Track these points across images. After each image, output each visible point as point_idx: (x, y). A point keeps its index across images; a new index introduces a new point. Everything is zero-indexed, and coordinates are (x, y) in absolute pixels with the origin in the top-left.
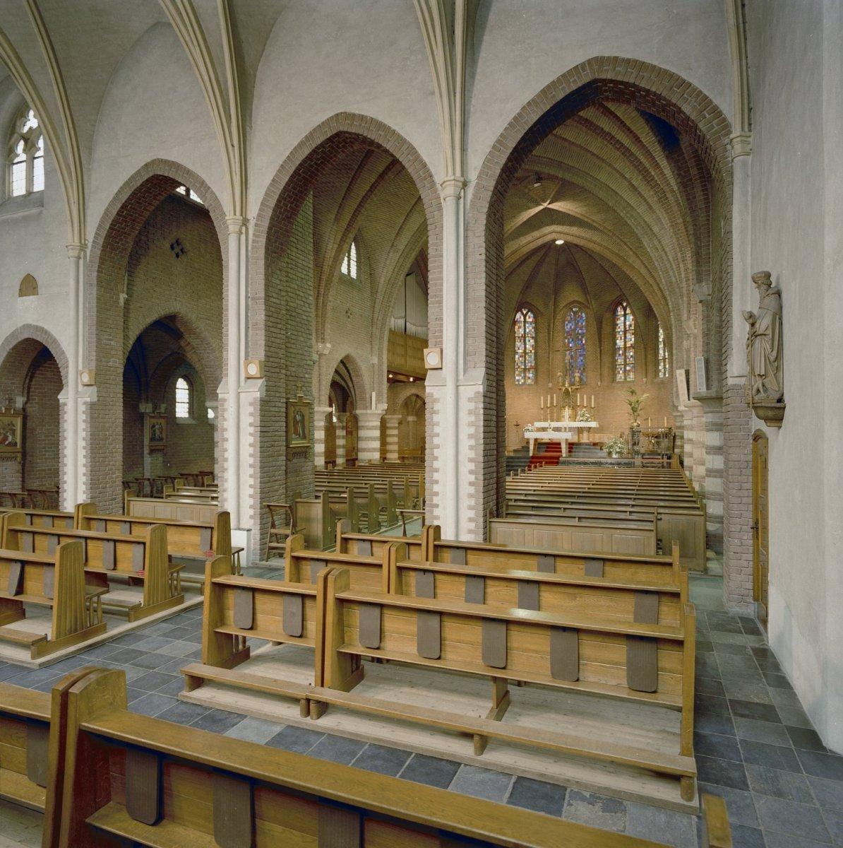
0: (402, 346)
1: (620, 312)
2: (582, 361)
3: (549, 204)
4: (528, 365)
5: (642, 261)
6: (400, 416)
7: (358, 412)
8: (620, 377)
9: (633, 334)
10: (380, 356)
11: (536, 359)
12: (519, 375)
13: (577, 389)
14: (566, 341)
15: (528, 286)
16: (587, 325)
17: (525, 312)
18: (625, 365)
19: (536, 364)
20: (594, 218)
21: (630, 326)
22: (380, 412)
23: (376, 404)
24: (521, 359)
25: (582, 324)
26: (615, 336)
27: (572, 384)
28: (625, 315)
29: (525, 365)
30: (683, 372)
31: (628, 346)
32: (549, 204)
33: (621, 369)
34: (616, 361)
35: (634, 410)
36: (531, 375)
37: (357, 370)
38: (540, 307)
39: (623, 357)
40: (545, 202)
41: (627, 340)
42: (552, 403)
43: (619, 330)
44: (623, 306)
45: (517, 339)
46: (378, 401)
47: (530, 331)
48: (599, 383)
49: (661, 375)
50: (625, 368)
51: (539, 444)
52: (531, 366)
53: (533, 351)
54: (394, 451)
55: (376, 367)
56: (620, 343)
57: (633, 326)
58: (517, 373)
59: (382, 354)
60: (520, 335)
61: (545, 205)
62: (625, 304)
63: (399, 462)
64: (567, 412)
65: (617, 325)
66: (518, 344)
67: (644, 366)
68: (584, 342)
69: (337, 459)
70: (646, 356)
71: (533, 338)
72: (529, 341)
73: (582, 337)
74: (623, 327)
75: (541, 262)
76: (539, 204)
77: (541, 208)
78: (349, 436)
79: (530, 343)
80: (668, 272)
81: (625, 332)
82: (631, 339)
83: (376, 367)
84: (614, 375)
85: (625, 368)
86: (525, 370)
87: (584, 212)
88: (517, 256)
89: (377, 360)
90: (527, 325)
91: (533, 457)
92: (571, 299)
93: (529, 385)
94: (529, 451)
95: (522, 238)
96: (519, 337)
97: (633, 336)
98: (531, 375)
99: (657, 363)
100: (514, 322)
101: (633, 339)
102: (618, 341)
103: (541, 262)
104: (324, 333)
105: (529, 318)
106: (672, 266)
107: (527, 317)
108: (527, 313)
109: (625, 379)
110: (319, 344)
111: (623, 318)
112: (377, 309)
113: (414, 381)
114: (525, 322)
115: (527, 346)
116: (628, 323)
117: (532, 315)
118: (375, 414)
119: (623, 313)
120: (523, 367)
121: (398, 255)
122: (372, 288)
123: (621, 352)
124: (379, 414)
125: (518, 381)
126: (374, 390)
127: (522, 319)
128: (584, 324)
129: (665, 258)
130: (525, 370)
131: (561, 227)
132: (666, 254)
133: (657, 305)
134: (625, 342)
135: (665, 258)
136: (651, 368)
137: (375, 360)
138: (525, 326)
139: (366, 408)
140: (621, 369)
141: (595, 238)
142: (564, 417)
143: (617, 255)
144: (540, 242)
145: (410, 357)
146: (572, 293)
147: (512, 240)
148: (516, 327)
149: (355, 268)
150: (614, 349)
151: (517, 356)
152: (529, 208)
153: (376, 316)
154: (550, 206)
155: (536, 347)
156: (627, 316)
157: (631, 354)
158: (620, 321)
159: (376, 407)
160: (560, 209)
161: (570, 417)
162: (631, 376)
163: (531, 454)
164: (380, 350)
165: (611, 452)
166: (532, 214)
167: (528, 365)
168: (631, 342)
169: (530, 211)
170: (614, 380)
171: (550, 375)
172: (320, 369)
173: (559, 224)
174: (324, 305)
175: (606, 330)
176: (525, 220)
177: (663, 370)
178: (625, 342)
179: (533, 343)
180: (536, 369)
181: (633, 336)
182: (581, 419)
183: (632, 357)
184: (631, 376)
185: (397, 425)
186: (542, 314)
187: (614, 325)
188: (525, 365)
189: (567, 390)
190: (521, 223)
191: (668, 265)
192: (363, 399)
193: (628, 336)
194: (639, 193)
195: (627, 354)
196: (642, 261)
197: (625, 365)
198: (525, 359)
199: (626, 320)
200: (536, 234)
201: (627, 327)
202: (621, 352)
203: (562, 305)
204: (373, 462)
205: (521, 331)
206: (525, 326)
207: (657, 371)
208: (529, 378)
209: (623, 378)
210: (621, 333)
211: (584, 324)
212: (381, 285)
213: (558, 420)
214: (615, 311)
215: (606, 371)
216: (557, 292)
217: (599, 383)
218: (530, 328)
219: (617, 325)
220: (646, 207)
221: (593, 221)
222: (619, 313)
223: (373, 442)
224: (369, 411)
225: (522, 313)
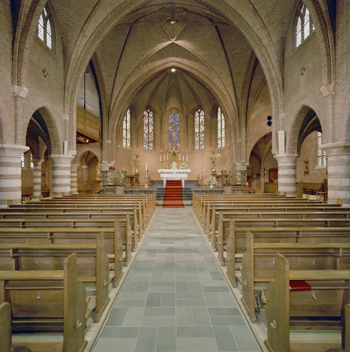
0: (83, 117)
1: (197, 114)
2: (177, 139)
3: (175, 40)
4: (150, 140)
5: (222, 81)
6: (79, 165)
7: (52, 156)
8: (197, 147)
9: (204, 126)
10: (71, 115)
11: (154, 136)
12: (146, 145)
13: (178, 152)
14: (170, 128)
15: (153, 95)
16: (180, 121)
17: (148, 111)
18: (200, 141)
19: (154, 139)
20: (199, 53)
21: (202, 121)
22: (71, 157)
23: (68, 151)
24: (146, 136)
25: (177, 120)
26: (194, 126)
27: (176, 149)
28: (199, 116)
29: (149, 140)
30: (283, 132)
31: (201, 132)
32: (175, 40)
33: (197, 143)
34: (195, 139)
35: (213, 162)
36: (152, 145)
37: (51, 122)
38: (157, 109)
39: (199, 137)
40: (173, 39)
41: (200, 129)
42: (163, 160)
43: (196, 124)
44: (198, 112)
45: (145, 126)
46: (69, 148)
47: (151, 121)
48: (186, 150)
49: (219, 146)
50: (200, 142)
51: (169, 182)
52: (152, 140)
53: (153, 132)
54: (284, 176)
55: (68, 123)
56: (197, 130)
57: (204, 122)
58: (144, 143)
59: (72, 113)
60: (146, 123)
61: (173, 40)
62: (199, 111)
63: (77, 193)
64: (174, 164)
65: (195, 121)
66: (145, 128)
67: (210, 142)
68: (178, 129)
69: (34, 193)
70: (211, 137)
71: (152, 125)
72: (151, 127)
73: (178, 127)
74: (198, 122)
75: (161, 82)
76: (169, 39)
77: (170, 42)
78: (44, 177)
79: (151, 128)
80: (271, 71)
81: (199, 125)
82: (203, 128)
83: (68, 123)
84: (194, 146)
85: (200, 142)
86: (149, 142)
87: (193, 49)
88: (152, 73)
89: (68, 117)
90: (150, 118)
91: (166, 189)
92: (173, 106)
93: (151, 150)
94: (163, 185)
95: (156, 62)
96: (145, 124)
97: (204, 127)
98: (152, 145)
99: (217, 140)
100: (144, 116)
101: (204, 128)
102: (196, 129)
103: (161, 82)
104: (20, 77)
105: (151, 114)
106: (273, 67)
107: (150, 114)
108: (149, 112)
109: (200, 148)
110: (15, 86)
111: (198, 118)
112: (68, 78)
113: (89, 142)
114: (148, 116)
115: (150, 129)
116: (201, 120)
117: (152, 113)
118: (68, 158)
119: (198, 115)
120: (148, 140)
121: (86, 40)
122: (64, 62)
123: (197, 135)
124: (70, 158)
125: (145, 148)
126: (65, 140)
127: (147, 115)
128: (178, 120)
129: (269, 61)
130: (149, 142)
131: (178, 58)
132: (270, 59)
133: (228, 106)
134: (199, 130)
135: (269, 61)
136: (213, 143)
137: (67, 117)
138: (148, 118)
139: (59, 153)
140: (197, 143)
141: (196, 67)
142: (173, 167)
143: (208, 78)
144: (161, 68)
145: (88, 125)
146: (173, 103)
147: (151, 62)
148: (144, 119)
149: (51, 41)
150: (194, 133)
151: (144, 135)
152: (163, 42)
153: (67, 84)
154: (175, 42)
155: (154, 130)
156: (201, 117)
157: (203, 136)
158: (197, 120)
159: (68, 153)
160: (181, 45)
161: (176, 167)
162: (203, 147)
163: (164, 187)
164: (71, 109)
165: (210, 184)
166: (165, 46)
167: (150, 140)
168: (203, 130)
169: (163, 43)
170: (194, 149)
171: (162, 146)
172: (16, 110)
173: (177, 56)
174: (21, 51)
175: (190, 123)
176: (160, 49)
177: (220, 144)
178: (199, 130)
179: (153, 128)
180: (154, 142)
181: (204, 127)
182: (183, 167)
183: (203, 137)
184: (203, 147)
185: (76, 170)
186: (157, 113)
187: (194, 121)
188: (149, 140)
189: (174, 152)
190: (157, 50)
191: (271, 66)
192: (58, 146)
193: (201, 127)
194: (259, 14)
195: (200, 136)
196: (222, 81)
197: (200, 141)
198: (149, 136)
199: (200, 118)
200: (164, 61)
201: (201, 122)
202: (197, 135)
203: (168, 109)
204: (66, 195)
205: (147, 121)
206: (148, 118)
207: (217, 144)
208: (151, 147)
209: (198, 148)
210: (197, 125)
211: (178, 120)
212: (72, 61)
213: (169, 168)
214: (194, 114)
215: (190, 144)
216: (167, 99)
217: (186, 150)
218: (151, 120)
219: (195, 121)
220: (262, 25)
221: (198, 55)
222: (196, 115)
223: (66, 179)
224: (62, 156)
225: (147, 112)
